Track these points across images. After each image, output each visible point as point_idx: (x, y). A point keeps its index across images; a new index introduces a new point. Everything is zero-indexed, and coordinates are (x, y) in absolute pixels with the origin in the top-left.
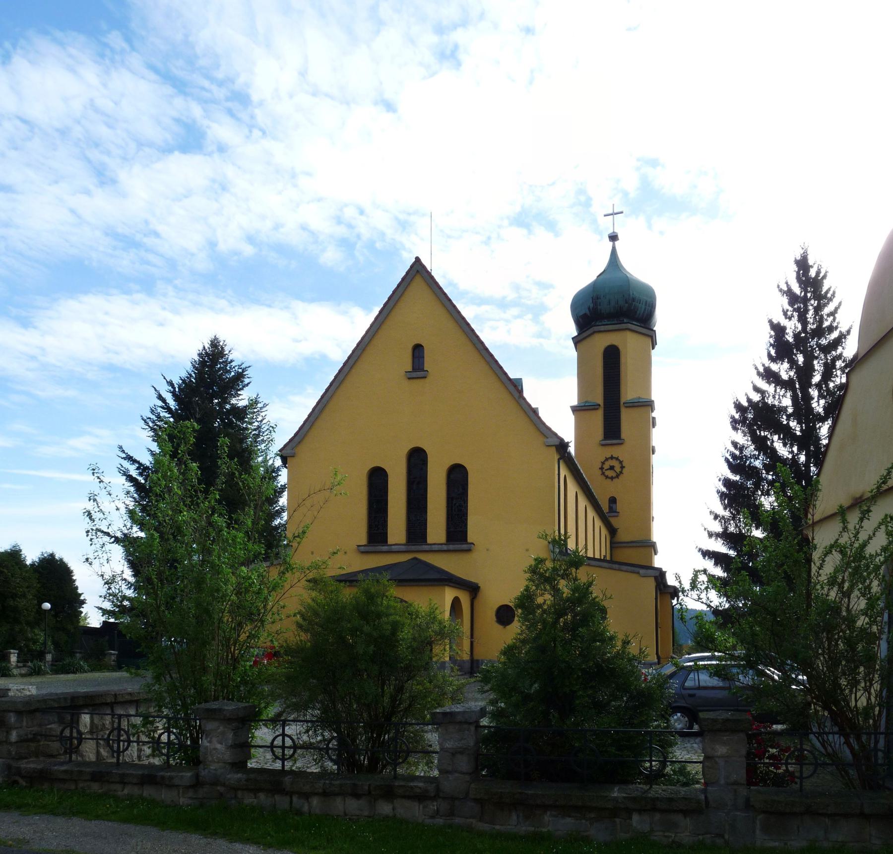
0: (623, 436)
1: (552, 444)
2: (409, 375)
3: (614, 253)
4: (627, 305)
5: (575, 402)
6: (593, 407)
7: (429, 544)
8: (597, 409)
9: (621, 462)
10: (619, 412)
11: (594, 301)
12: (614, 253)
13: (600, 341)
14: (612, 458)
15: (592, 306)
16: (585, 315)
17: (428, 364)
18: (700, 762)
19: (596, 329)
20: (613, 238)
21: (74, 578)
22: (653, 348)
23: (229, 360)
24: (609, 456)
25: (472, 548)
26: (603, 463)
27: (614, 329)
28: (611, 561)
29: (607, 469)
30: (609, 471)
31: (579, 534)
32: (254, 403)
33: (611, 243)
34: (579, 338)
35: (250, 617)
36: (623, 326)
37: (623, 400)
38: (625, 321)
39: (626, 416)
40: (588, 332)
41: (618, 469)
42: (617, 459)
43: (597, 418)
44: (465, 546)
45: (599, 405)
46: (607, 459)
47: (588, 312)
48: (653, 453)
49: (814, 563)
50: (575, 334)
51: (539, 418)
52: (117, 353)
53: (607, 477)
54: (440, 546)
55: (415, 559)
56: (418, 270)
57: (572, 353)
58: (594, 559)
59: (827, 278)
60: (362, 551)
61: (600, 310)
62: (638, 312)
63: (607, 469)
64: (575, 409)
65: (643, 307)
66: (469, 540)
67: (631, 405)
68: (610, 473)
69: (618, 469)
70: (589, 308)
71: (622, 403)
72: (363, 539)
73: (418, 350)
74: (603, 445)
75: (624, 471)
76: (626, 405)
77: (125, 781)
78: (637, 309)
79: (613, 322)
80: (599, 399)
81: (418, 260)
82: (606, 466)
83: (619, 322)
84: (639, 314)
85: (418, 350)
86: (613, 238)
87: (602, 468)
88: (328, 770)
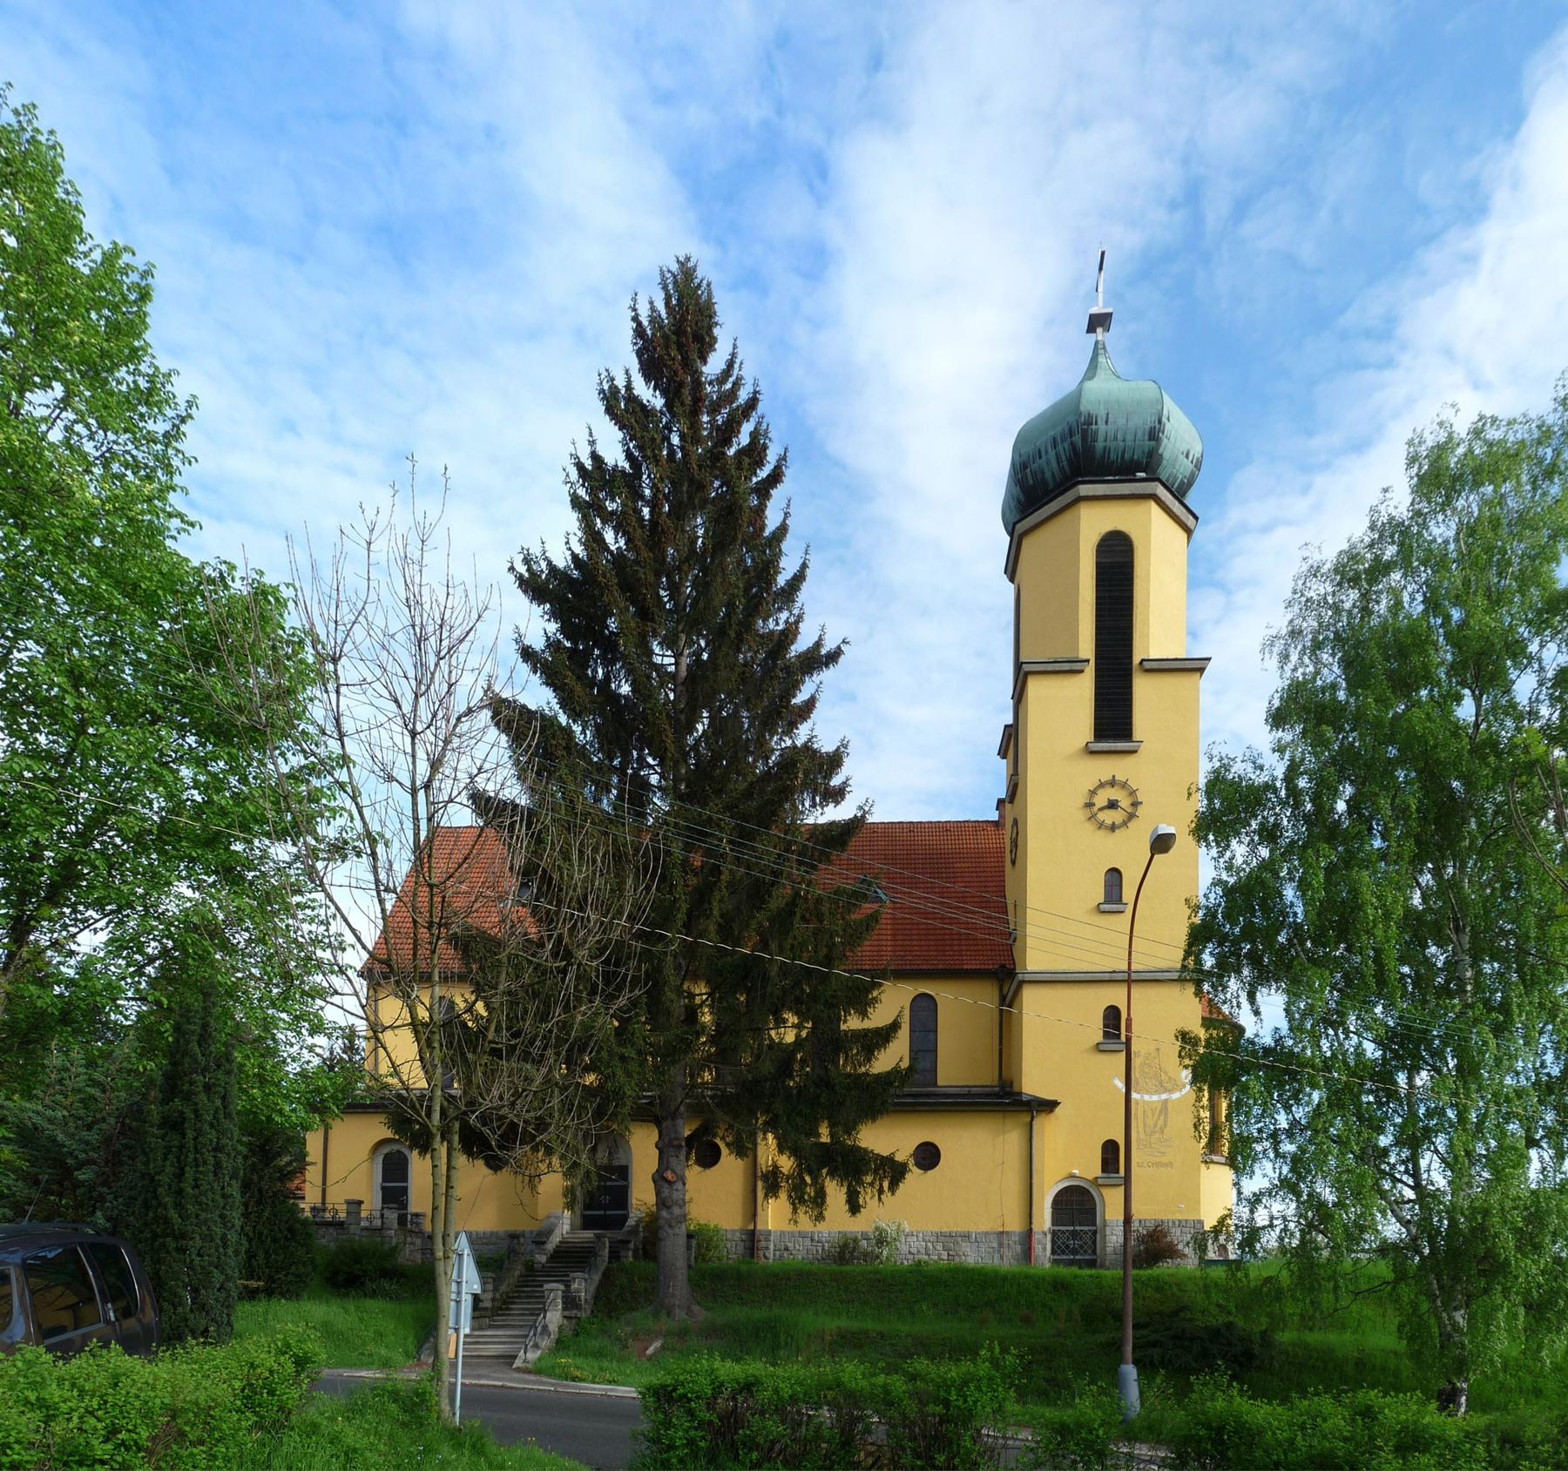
9: (1133, 793)
14: (1113, 783)
18: (324, 1203)
23: (801, 644)
24: (1106, 777)
26: (1093, 793)
29: (1101, 809)
30: (1106, 811)
32: (845, 784)
35: (732, 1420)
37: (1136, 660)
42: (1124, 785)
46: (1102, 785)
53: (1101, 825)
62: (1048, 475)
67: (1066, 667)
68: (1109, 817)
69: (1125, 803)
76: (1147, 665)
82: (1101, 799)
84: (1053, 474)
87: (1090, 805)
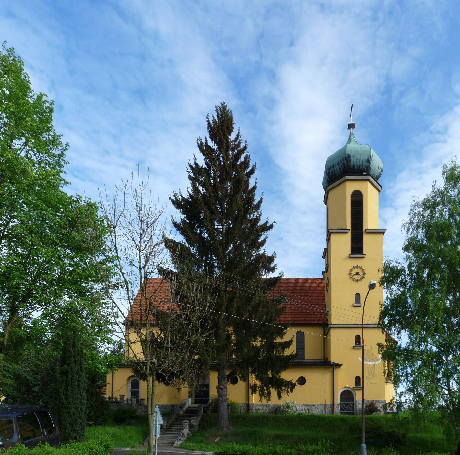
0: (365, 252)
8: (347, 233)
9: (363, 270)
14: (357, 267)
21: (69, 195)
24: (355, 265)
26: (351, 270)
27: (360, 179)
29: (354, 275)
31: (342, 323)
41: (361, 273)
42: (361, 268)
46: (354, 268)
52: (327, 291)
53: (354, 280)
62: (336, 173)
63: (354, 275)
68: (356, 277)
69: (361, 273)
75: (366, 276)
76: (367, 231)
82: (354, 272)
84: (338, 173)
87: (350, 274)
88: (45, 102)
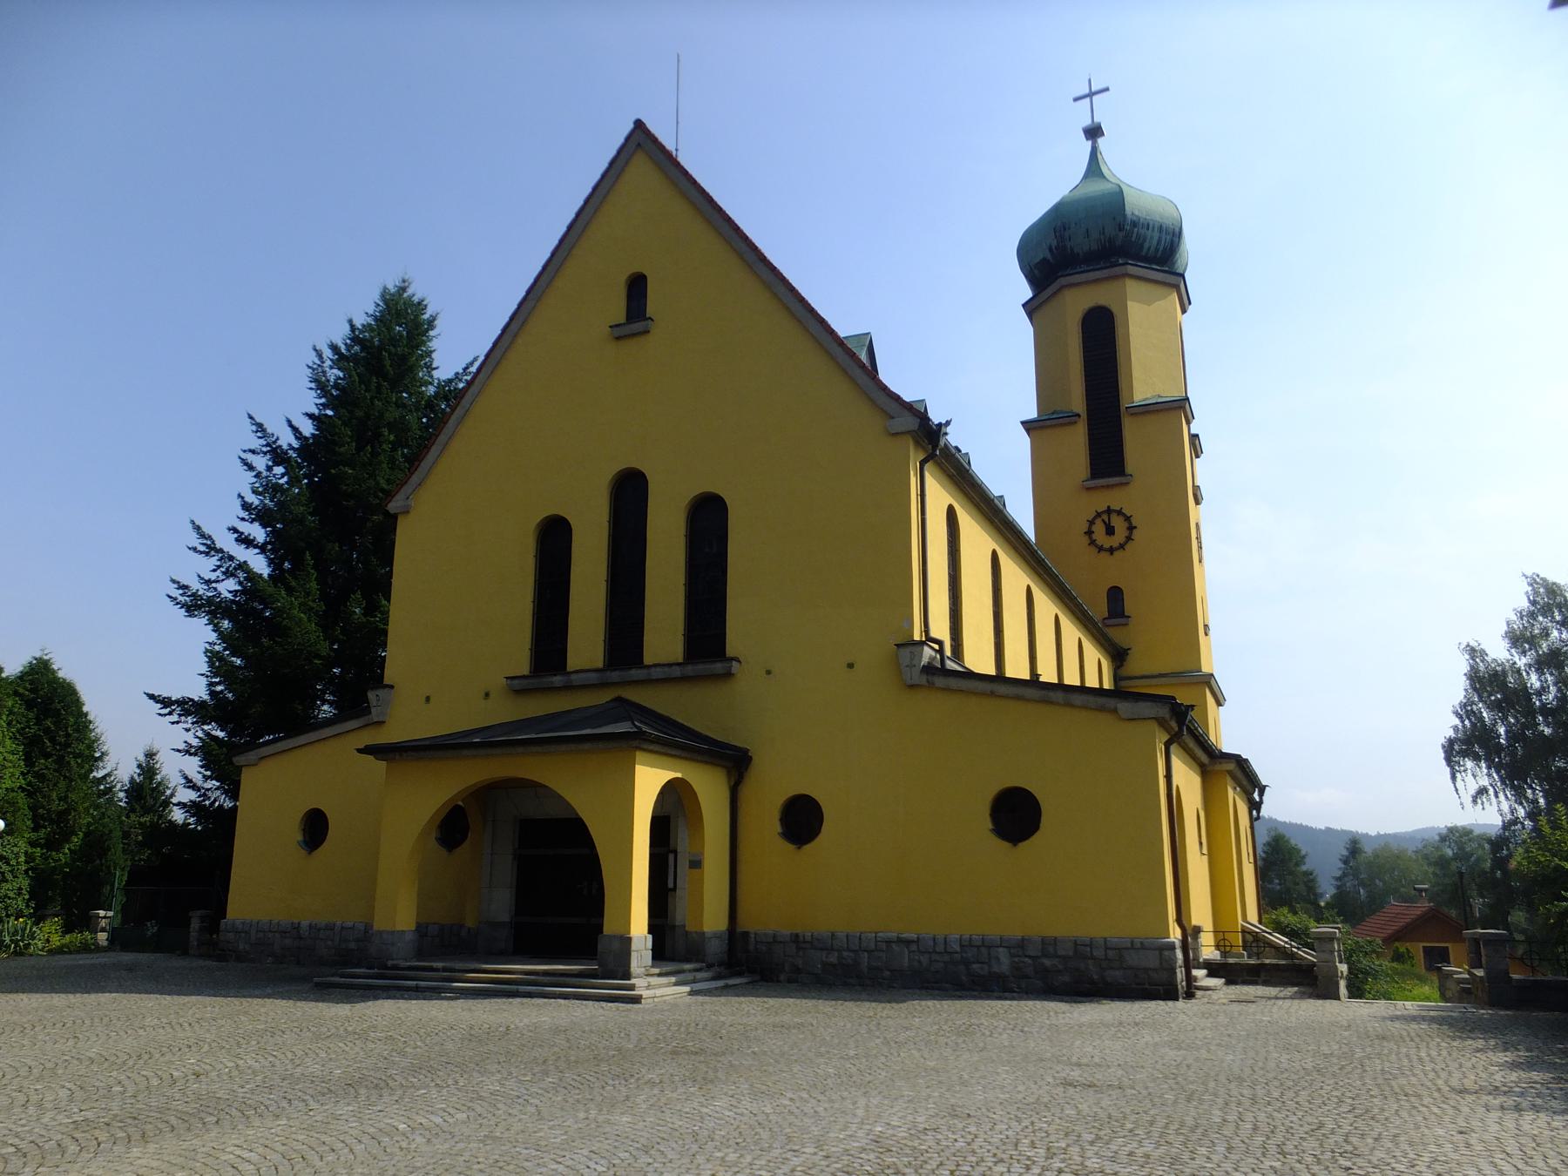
0: (1129, 469)
1: (903, 429)
2: (619, 332)
3: (1094, 154)
4: (1121, 234)
5: (1032, 413)
6: (1070, 418)
7: (649, 667)
10: (1120, 425)
11: (1058, 234)
12: (1094, 154)
13: (1076, 301)
15: (1054, 243)
16: (1044, 260)
17: (1129, 606)
19: (1063, 281)
20: (1094, 132)
22: (1184, 311)
25: (734, 670)
28: (1118, 693)
33: (1090, 143)
34: (1036, 303)
36: (1117, 270)
37: (1125, 404)
38: (1121, 261)
39: (1133, 435)
40: (1049, 291)
43: (1077, 440)
44: (718, 667)
45: (1079, 415)
47: (1049, 256)
48: (1197, 502)
49: (1282, 991)
50: (1027, 293)
51: (884, 388)
54: (666, 669)
55: (619, 699)
56: (641, 140)
57: (1024, 332)
58: (1082, 689)
59: (1444, 762)
60: (519, 688)
61: (1072, 250)
62: (1146, 245)
64: (1029, 426)
65: (1156, 235)
66: (730, 652)
70: (1050, 249)
71: (1123, 409)
72: (523, 666)
73: (637, 286)
74: (1088, 489)
76: (1131, 410)
77: (932, 944)
78: (1145, 240)
79: (1098, 266)
80: (1077, 401)
81: (639, 124)
83: (1108, 265)
85: (637, 286)
86: (1094, 132)
